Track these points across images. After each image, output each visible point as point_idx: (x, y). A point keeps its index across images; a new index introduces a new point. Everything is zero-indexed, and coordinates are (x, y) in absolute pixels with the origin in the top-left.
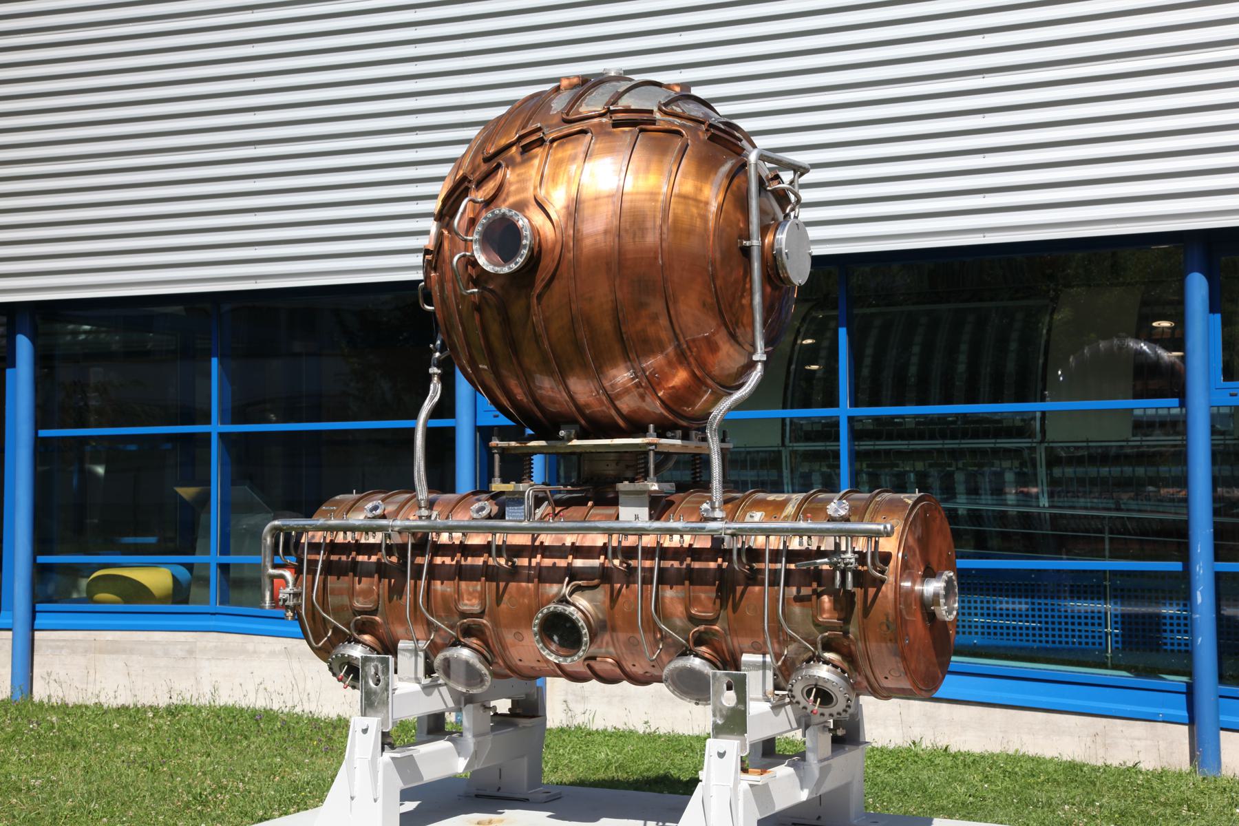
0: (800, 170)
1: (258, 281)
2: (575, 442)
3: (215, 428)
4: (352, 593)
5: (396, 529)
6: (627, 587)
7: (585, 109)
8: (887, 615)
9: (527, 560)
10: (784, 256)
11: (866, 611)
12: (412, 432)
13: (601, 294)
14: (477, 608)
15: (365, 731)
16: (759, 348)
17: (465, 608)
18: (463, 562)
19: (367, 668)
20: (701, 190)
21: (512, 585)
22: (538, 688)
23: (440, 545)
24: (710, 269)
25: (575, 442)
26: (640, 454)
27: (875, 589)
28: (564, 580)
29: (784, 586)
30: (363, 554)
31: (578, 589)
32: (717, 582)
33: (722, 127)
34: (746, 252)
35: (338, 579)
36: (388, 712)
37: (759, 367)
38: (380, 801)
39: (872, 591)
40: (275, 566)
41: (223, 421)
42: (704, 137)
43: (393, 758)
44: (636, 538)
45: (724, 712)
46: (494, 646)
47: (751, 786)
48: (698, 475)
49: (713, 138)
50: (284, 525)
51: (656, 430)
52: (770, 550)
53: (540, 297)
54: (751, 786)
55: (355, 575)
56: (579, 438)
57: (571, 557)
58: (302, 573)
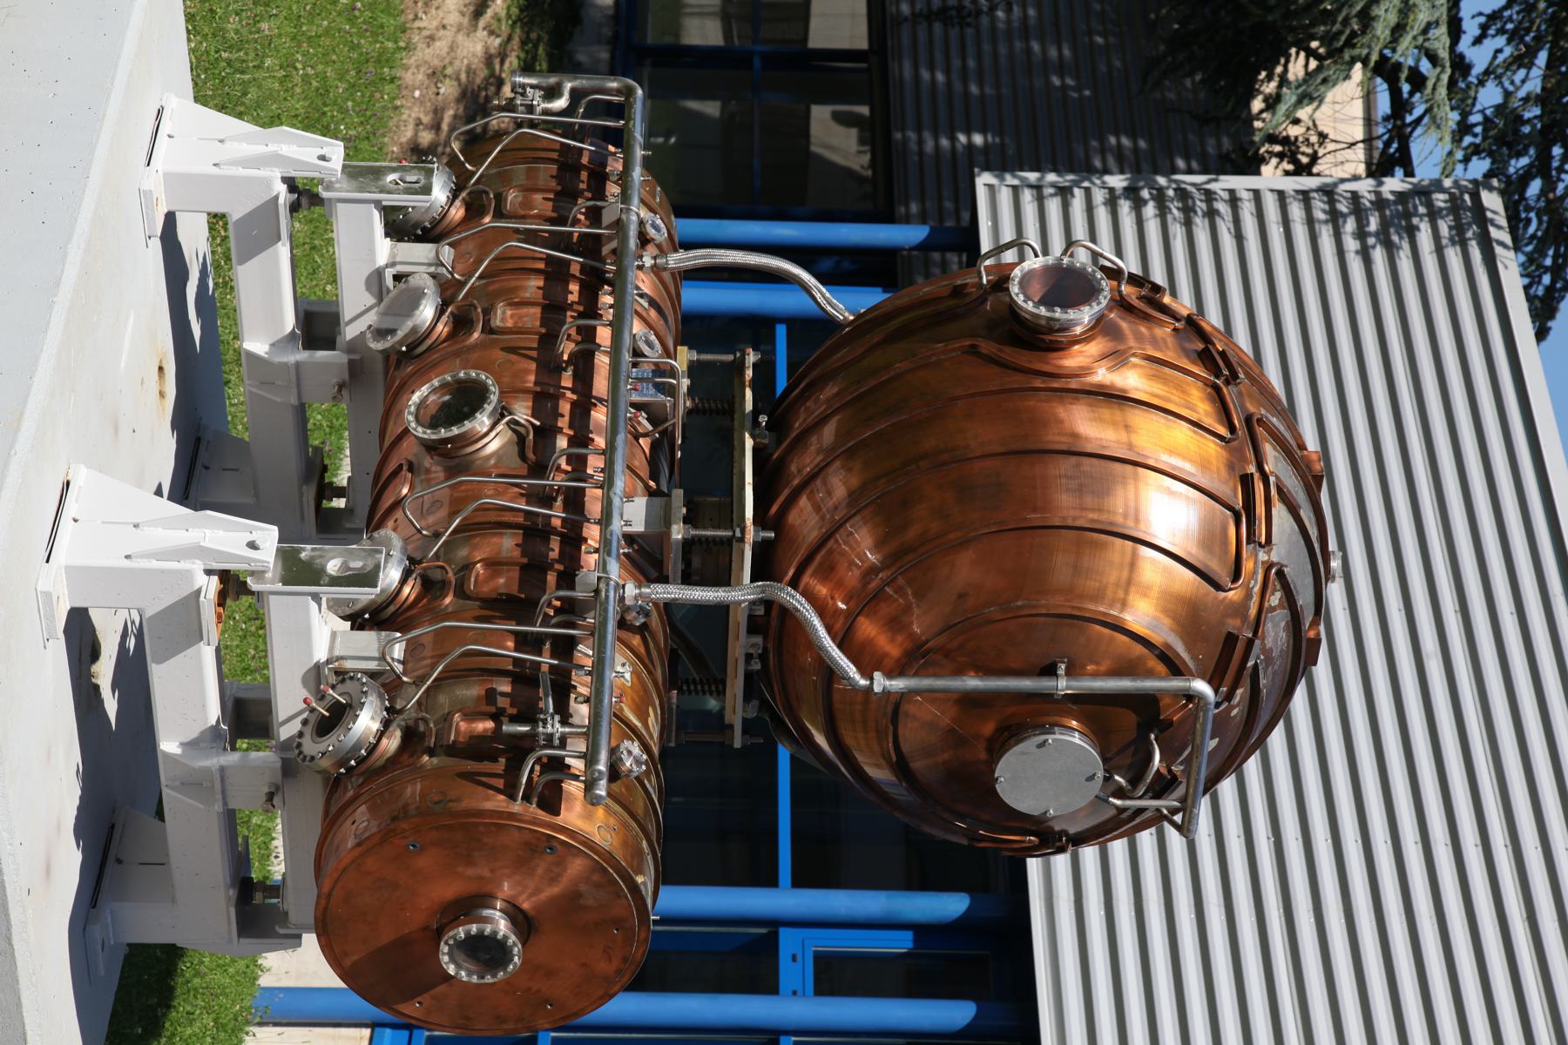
0: (1185, 829)
2: (749, 443)
4: (529, 190)
5: (624, 217)
6: (522, 495)
7: (1270, 451)
8: (458, 800)
9: (570, 386)
10: (1042, 738)
11: (470, 777)
12: (766, 878)
13: (982, 434)
14: (497, 322)
15: (252, 545)
16: (894, 683)
17: (499, 312)
18: (569, 313)
19: (416, 171)
20: (1145, 595)
21: (533, 366)
22: (299, 937)
23: (598, 294)
24: (1019, 603)
25: (749, 443)
26: (729, 513)
27: (502, 787)
28: (538, 420)
29: (514, 658)
30: (580, 292)
31: (521, 440)
32: (523, 596)
33: (1250, 664)
34: (1050, 671)
35: (552, 177)
36: (349, 191)
37: (863, 682)
38: (215, 170)
39: (500, 783)
40: (573, 92)
42: (1233, 624)
43: (276, 198)
44: (588, 662)
45: (318, 561)
46: (435, 353)
47: (198, 592)
48: (692, 687)
49: (1231, 639)
50: (635, 99)
51: (765, 542)
52: (583, 489)
53: (973, 351)
54: (198, 592)
55: (557, 194)
56: (755, 450)
57: (571, 433)
58: (552, 224)
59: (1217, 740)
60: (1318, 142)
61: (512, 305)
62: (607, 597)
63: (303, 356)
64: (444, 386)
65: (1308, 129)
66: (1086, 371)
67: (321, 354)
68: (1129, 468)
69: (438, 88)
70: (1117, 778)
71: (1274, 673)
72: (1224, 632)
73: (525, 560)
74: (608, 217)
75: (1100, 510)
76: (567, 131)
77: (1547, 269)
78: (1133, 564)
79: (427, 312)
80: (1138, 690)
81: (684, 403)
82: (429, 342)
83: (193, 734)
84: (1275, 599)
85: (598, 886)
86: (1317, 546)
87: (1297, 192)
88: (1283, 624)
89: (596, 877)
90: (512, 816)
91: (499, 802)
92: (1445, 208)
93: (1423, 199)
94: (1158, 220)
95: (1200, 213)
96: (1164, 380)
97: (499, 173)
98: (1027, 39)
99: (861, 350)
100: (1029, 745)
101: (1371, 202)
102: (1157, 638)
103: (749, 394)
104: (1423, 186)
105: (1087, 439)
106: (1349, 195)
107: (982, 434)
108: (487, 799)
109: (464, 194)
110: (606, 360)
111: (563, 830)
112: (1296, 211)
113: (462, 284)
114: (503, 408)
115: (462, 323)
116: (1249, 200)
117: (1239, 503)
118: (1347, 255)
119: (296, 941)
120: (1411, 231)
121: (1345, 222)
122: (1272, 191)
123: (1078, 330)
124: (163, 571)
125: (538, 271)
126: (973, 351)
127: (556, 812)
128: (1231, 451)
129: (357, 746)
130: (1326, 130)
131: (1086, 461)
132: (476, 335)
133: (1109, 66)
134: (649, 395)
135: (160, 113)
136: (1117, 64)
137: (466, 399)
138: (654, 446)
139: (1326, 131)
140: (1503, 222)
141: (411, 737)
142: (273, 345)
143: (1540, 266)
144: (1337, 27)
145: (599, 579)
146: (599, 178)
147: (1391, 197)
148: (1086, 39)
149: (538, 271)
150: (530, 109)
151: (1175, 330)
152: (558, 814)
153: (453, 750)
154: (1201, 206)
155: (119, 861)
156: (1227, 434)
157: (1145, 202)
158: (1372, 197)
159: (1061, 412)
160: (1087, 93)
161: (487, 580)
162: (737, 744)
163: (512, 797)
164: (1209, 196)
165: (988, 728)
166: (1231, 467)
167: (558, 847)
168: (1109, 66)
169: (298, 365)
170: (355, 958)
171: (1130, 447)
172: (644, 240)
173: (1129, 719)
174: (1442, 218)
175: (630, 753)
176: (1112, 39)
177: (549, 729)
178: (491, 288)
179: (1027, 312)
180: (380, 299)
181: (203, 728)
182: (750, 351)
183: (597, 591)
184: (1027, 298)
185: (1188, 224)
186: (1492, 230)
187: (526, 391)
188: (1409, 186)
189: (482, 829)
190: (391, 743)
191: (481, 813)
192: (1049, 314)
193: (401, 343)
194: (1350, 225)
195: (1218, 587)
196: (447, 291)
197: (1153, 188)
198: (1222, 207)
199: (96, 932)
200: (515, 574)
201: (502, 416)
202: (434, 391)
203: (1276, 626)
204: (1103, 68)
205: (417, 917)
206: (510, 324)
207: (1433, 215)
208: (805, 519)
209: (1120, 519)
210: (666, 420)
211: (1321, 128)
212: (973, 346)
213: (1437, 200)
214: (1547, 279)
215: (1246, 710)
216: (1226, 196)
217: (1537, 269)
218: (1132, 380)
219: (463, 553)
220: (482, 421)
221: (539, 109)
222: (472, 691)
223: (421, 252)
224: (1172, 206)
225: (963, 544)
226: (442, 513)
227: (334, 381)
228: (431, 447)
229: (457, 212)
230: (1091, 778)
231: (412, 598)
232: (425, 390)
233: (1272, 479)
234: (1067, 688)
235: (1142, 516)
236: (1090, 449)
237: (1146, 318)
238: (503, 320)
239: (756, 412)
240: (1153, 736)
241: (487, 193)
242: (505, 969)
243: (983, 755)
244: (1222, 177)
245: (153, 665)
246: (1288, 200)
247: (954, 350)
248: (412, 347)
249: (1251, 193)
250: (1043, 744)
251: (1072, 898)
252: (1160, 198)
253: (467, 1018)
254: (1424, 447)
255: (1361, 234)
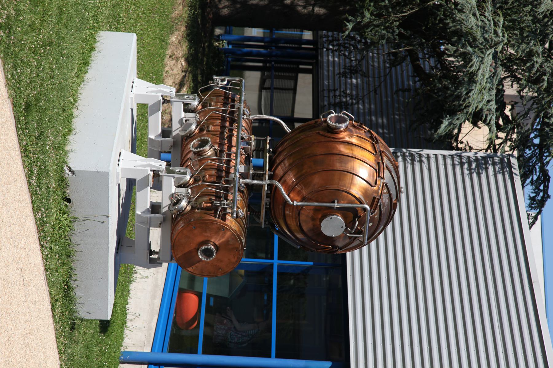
1: (351, 276)
2: (268, 155)
3: (276, 262)
11: (206, 213)
13: (319, 150)
21: (218, 138)
22: (162, 264)
25: (268, 155)
33: (379, 204)
34: (334, 202)
37: (292, 203)
38: (147, 93)
39: (213, 215)
41: (279, 267)
42: (375, 195)
43: (160, 100)
47: (149, 175)
49: (374, 198)
51: (271, 174)
53: (319, 133)
54: (149, 175)
55: (224, 103)
56: (269, 157)
59: (372, 223)
60: (469, 149)
61: (213, 126)
62: (236, 179)
63: (163, 139)
64: (199, 141)
65: (466, 145)
66: (344, 138)
67: (167, 139)
68: (352, 158)
69: (163, 117)
70: (348, 229)
71: (386, 209)
72: (373, 196)
73: (217, 175)
74: (236, 107)
75: (345, 167)
76: (225, 88)
77: (541, 191)
78: (352, 179)
79: (193, 127)
80: (352, 206)
81: (253, 148)
82: (194, 133)
83: (144, 210)
84: (385, 191)
85: (233, 239)
86: (397, 183)
87: (450, 155)
88: (387, 197)
89: (233, 237)
90: (215, 221)
91: (213, 218)
92: (498, 162)
93: (491, 159)
94: (403, 162)
95: (416, 161)
96: (361, 141)
97: (210, 99)
98: (371, 116)
99: (294, 135)
100: (328, 218)
101: (474, 159)
102: (357, 196)
103: (268, 145)
104: (491, 155)
105: (343, 152)
106: (467, 157)
107: (319, 150)
108: (210, 217)
109: (201, 103)
110: (236, 139)
111: (226, 225)
112: (449, 161)
113: (201, 122)
114: (212, 146)
115: (201, 130)
116: (434, 157)
117: (377, 168)
118: (465, 175)
119: (160, 265)
120: (487, 169)
121: (464, 165)
122: (441, 155)
123: (342, 129)
124: (142, 170)
125: (219, 119)
126: (319, 133)
127: (225, 221)
128: (376, 157)
129: (182, 208)
130: (472, 146)
131: (343, 156)
132: (205, 132)
133: (401, 126)
134: (245, 146)
135: (133, 81)
136: (403, 125)
137: (204, 143)
138: (246, 158)
139: (472, 146)
140: (517, 167)
141: (193, 208)
142: (155, 136)
143: (539, 189)
144: (461, 102)
145: (234, 176)
146: (233, 101)
147: (480, 158)
148: (392, 117)
149: (219, 119)
150: (218, 84)
151: (365, 132)
152: (225, 221)
153: (202, 209)
154: (417, 159)
155: (122, 246)
156: (375, 153)
157: (398, 157)
158: (474, 158)
159: (338, 146)
160: (392, 135)
161: (209, 179)
162: (263, 227)
163: (216, 217)
164: (420, 156)
165: (320, 216)
166: (375, 160)
167: (225, 229)
168: (401, 126)
169: (161, 141)
170: (179, 256)
171: (353, 154)
172: (244, 114)
173: (351, 215)
174: (497, 165)
175: (240, 212)
176: (402, 117)
177: (224, 202)
178: (208, 122)
179: (331, 124)
180: (182, 125)
181: (146, 208)
182: (269, 137)
183: (234, 179)
184: (331, 121)
185: (413, 164)
186: (513, 170)
187: (217, 143)
188: (486, 155)
189: (209, 224)
190: (188, 208)
191: (209, 220)
192: (335, 125)
193: (187, 133)
194: (466, 166)
195: (371, 186)
196: (198, 123)
197: (402, 153)
198: (424, 159)
199: (118, 258)
200: (215, 177)
201: (212, 147)
202: (197, 141)
203: (385, 197)
204: (398, 127)
205: (193, 246)
206: (213, 129)
207: (494, 164)
208: (280, 171)
209: (350, 169)
210: (249, 151)
211: (470, 145)
212: (319, 132)
213: (496, 159)
214: (541, 194)
215: (379, 217)
216: (426, 156)
217: (538, 191)
218: (354, 140)
219: (203, 173)
220: (207, 147)
221: (220, 84)
222: (206, 199)
223: (192, 115)
224: (407, 158)
225: (315, 173)
226: (198, 167)
227: (170, 145)
228: (195, 153)
229: (200, 107)
230: (342, 227)
231: (192, 183)
232: (194, 141)
233: (385, 164)
234: (337, 206)
235: (355, 169)
236: (343, 154)
237: (358, 129)
238: (211, 129)
239: (270, 148)
240: (356, 219)
241: (207, 103)
242: (212, 257)
243: (318, 223)
244: (424, 150)
245: (137, 192)
246: (446, 157)
247: (315, 133)
248: (190, 135)
249: (434, 155)
250: (331, 218)
251: (364, 362)
252: (404, 156)
253: (203, 272)
254: (486, 235)
255: (470, 169)
